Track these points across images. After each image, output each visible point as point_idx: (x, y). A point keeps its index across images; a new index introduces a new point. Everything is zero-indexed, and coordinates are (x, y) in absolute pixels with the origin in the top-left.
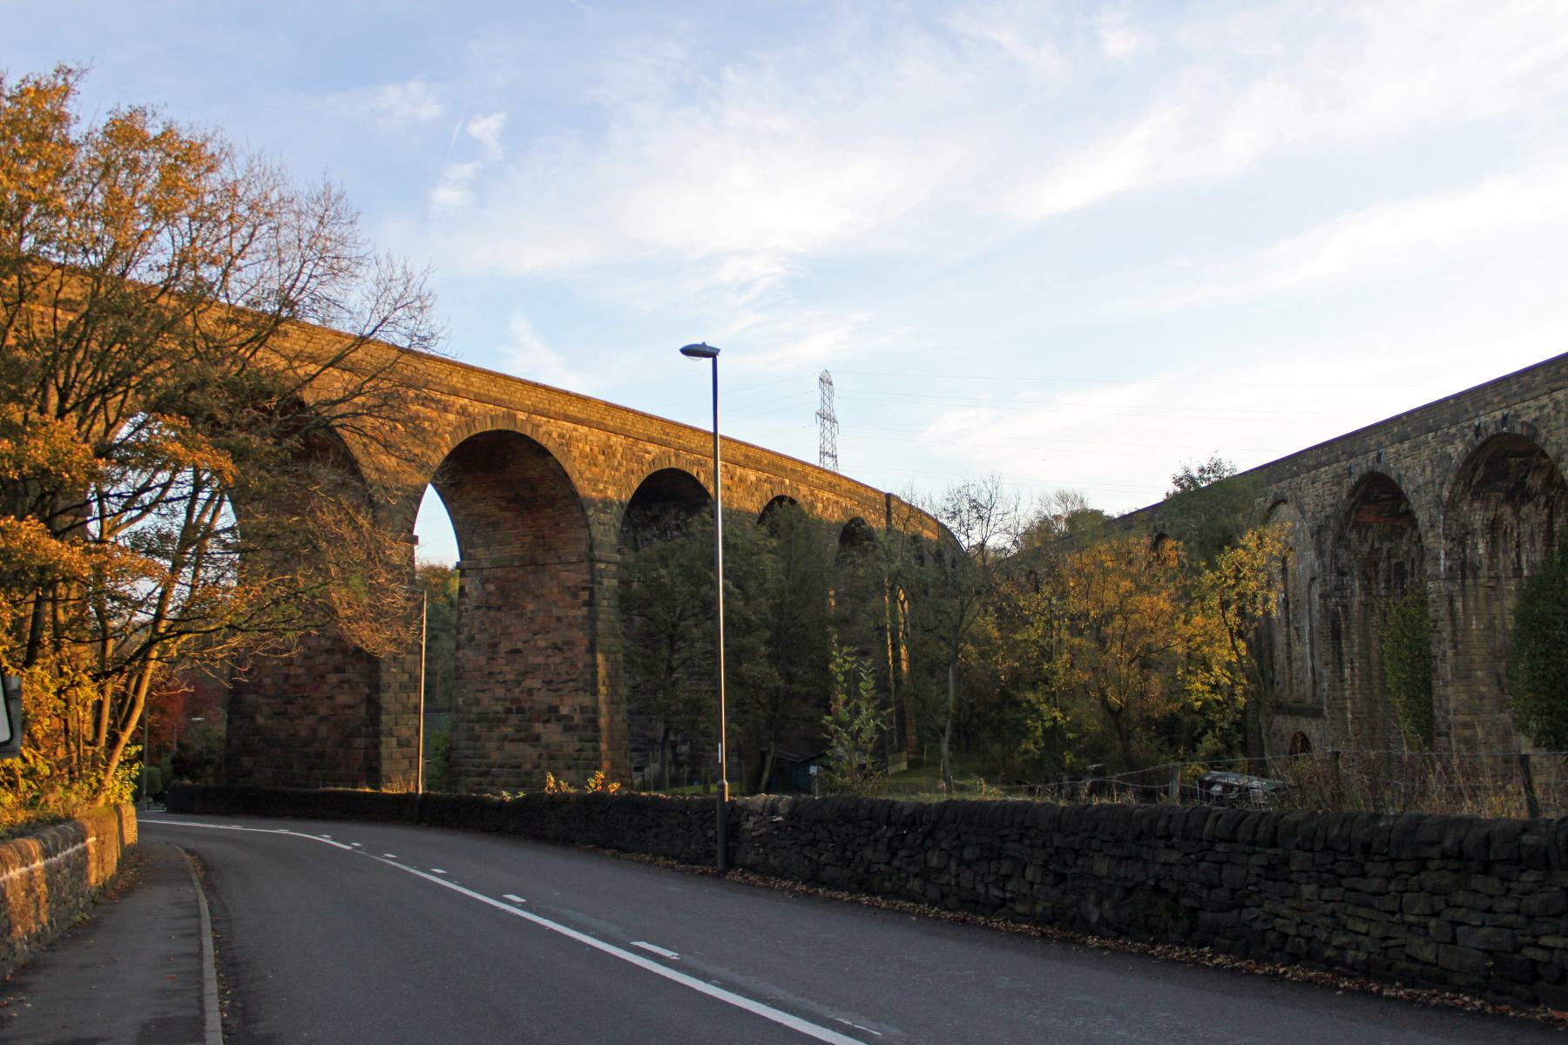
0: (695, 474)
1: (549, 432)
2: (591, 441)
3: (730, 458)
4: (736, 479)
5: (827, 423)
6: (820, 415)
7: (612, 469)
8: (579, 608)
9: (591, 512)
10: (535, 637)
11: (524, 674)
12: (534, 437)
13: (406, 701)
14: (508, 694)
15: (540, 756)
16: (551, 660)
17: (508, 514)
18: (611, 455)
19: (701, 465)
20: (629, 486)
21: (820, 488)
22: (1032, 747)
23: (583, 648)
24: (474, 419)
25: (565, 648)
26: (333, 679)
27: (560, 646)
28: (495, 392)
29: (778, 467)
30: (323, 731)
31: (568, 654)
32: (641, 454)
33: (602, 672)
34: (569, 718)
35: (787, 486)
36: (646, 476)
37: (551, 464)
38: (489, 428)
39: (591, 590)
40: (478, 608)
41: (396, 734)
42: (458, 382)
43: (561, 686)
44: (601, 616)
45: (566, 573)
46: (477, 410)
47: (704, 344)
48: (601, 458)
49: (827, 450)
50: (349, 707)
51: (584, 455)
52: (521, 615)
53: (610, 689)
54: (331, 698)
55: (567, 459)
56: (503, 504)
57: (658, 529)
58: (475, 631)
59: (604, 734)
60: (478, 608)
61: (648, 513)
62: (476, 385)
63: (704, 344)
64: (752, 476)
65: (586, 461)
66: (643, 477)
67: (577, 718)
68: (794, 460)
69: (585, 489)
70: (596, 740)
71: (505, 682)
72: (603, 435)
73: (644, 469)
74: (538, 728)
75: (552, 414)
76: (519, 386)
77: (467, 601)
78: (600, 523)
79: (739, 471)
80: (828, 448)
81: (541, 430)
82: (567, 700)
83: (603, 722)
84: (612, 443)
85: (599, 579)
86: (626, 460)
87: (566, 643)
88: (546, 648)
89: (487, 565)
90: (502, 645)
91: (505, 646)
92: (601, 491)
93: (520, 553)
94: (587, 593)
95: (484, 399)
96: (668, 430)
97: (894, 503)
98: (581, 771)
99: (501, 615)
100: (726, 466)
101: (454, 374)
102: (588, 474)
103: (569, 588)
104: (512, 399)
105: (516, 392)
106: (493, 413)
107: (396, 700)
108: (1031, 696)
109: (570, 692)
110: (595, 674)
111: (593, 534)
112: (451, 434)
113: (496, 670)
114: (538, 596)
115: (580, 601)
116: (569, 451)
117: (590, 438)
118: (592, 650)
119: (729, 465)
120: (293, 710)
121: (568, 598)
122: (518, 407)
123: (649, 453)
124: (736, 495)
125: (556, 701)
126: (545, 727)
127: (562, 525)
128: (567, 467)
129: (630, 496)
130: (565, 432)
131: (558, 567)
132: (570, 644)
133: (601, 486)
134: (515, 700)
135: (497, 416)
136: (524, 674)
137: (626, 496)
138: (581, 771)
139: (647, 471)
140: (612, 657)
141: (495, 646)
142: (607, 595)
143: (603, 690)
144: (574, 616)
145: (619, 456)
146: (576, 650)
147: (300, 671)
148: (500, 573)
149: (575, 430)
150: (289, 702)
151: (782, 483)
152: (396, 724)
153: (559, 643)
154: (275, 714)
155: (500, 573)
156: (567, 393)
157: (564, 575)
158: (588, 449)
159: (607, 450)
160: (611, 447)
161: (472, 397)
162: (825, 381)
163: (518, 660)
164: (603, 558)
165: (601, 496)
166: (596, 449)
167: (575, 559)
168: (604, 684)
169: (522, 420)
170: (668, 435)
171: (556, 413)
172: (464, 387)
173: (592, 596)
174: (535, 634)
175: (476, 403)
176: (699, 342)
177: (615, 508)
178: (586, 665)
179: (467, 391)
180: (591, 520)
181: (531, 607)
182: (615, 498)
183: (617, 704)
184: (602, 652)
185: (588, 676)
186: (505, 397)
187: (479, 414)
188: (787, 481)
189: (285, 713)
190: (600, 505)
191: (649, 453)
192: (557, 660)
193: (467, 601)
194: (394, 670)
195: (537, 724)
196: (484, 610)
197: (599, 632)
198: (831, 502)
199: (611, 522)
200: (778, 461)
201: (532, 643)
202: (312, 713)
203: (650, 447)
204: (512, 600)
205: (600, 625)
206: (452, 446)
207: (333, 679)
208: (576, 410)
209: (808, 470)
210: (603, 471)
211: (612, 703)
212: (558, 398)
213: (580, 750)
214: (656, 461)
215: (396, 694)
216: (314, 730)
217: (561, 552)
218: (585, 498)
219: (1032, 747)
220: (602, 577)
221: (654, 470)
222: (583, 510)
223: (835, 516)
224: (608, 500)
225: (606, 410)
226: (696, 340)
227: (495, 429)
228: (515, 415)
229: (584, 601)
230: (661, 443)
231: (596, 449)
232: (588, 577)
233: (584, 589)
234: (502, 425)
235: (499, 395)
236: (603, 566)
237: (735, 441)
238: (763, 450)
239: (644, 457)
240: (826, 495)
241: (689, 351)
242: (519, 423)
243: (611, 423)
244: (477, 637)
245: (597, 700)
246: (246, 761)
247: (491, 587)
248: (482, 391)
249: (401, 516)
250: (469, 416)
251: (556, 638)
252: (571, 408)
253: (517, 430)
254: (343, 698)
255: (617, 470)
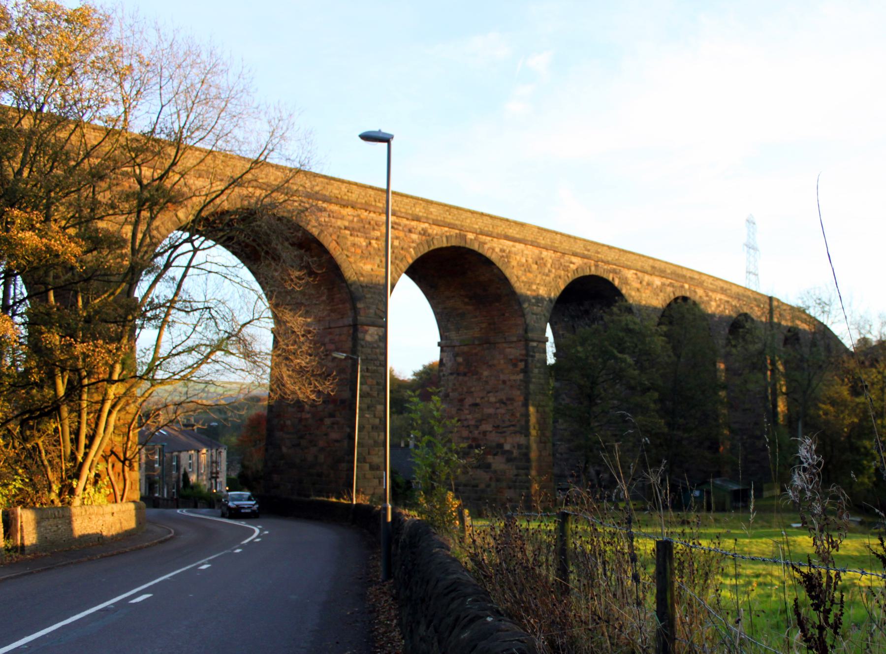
0: (610, 279)
1: (493, 248)
2: (527, 254)
3: (639, 268)
4: (644, 283)
5: (751, 251)
6: (747, 245)
7: (544, 274)
8: (518, 374)
9: (526, 305)
10: (489, 395)
11: (480, 421)
12: (480, 251)
13: (377, 438)
14: (470, 435)
15: (491, 479)
16: (499, 411)
17: (470, 308)
18: (542, 265)
19: (616, 273)
20: (557, 287)
21: (713, 291)
22: (866, 480)
23: (520, 403)
24: (433, 238)
25: (509, 402)
26: (328, 421)
27: (505, 401)
28: (449, 219)
29: (678, 275)
30: (322, 458)
31: (510, 407)
32: (567, 264)
33: (533, 420)
34: (510, 452)
35: (686, 289)
36: (571, 280)
37: (495, 271)
38: (445, 245)
39: (526, 361)
40: (451, 374)
41: (368, 461)
42: (420, 211)
43: (505, 429)
44: (534, 380)
45: (510, 349)
46: (435, 232)
47: (380, 131)
48: (535, 267)
49: (751, 270)
50: (337, 441)
51: (520, 265)
52: (479, 379)
53: (539, 432)
54: (326, 435)
55: (507, 268)
56: (466, 300)
57: (589, 319)
58: (449, 390)
59: (534, 464)
60: (451, 374)
61: (581, 308)
62: (434, 213)
63: (380, 131)
64: (657, 281)
65: (523, 269)
66: (568, 281)
67: (516, 453)
68: (692, 271)
69: (520, 287)
70: (528, 468)
71: (468, 426)
72: (536, 251)
73: (569, 275)
74: (490, 458)
75: (495, 234)
76: (469, 215)
77: (444, 369)
78: (533, 314)
79: (647, 278)
80: (752, 269)
81: (486, 246)
82: (509, 440)
83: (534, 455)
84: (543, 256)
85: (531, 353)
86: (555, 268)
87: (508, 399)
88: (496, 403)
89: (457, 344)
90: (467, 400)
91: (469, 401)
92: (534, 291)
93: (478, 335)
94: (523, 363)
95: (441, 223)
96: (589, 248)
97: (775, 303)
98: (518, 490)
99: (466, 379)
100: (636, 274)
101: (417, 206)
102: (524, 278)
103: (511, 360)
104: (463, 224)
105: (466, 219)
106: (448, 234)
107: (369, 437)
108: (867, 443)
109: (511, 433)
110: (528, 421)
111: (528, 321)
112: (414, 248)
113: (463, 417)
114: (490, 366)
115: (518, 369)
116: (509, 262)
117: (526, 252)
118: (526, 405)
119: (640, 274)
120: (304, 442)
121: (511, 367)
122: (468, 229)
123: (574, 263)
124: (644, 295)
125: (502, 441)
126: (494, 459)
127: (507, 315)
128: (507, 273)
129: (558, 294)
130: (505, 248)
131: (505, 345)
132: (511, 400)
133: (534, 287)
134: (474, 439)
135: (451, 236)
136: (480, 421)
137: (554, 294)
138: (518, 490)
139: (571, 277)
140: (540, 409)
141: (461, 401)
142: (539, 365)
143: (533, 432)
144: (514, 380)
145: (549, 265)
146: (515, 404)
147: (308, 416)
148: (466, 349)
149: (514, 246)
150: (301, 437)
151: (682, 287)
152: (369, 453)
153: (504, 398)
154: (293, 445)
155: (466, 349)
156: (507, 220)
157: (508, 350)
158: (524, 260)
159: (540, 262)
160: (543, 259)
161: (431, 222)
162: (750, 222)
163: (477, 410)
164: (535, 339)
165: (534, 294)
166: (530, 261)
167: (515, 339)
168: (534, 428)
169: (471, 240)
170: (589, 250)
171: (498, 234)
172: (425, 215)
173: (526, 366)
174: (489, 392)
175: (434, 227)
176: (376, 129)
177: (545, 303)
178: (522, 415)
179: (427, 218)
180: (526, 311)
181: (486, 373)
182: (546, 296)
183: (545, 443)
184: (533, 405)
185: (523, 423)
186: (457, 222)
187: (437, 234)
188: (686, 286)
189: (299, 445)
190: (533, 301)
191: (574, 263)
192: (502, 411)
193: (444, 369)
194: (367, 416)
195: (489, 457)
196: (455, 376)
197: (531, 392)
198: (723, 301)
199: (542, 313)
200: (679, 271)
201: (486, 399)
202: (315, 445)
203: (574, 259)
204: (473, 368)
205: (532, 387)
206: (415, 258)
207: (328, 421)
208: (515, 232)
209: (704, 278)
210: (536, 276)
211: (541, 442)
212: (499, 223)
213: (516, 475)
214: (579, 270)
215: (369, 433)
216: (316, 457)
217: (507, 334)
218: (522, 295)
219: (866, 480)
220: (534, 352)
221: (577, 276)
222: (520, 304)
223: (658, 302)
224: (540, 297)
225: (539, 232)
226: (372, 127)
227: (449, 245)
228: (465, 236)
229: (522, 369)
230: (584, 257)
231: (530, 261)
232: (524, 352)
233: (521, 361)
234: (454, 243)
235: (452, 221)
236: (535, 344)
237: (644, 256)
238: (666, 263)
239: (569, 266)
240: (719, 296)
241: (367, 137)
242: (468, 241)
243: (543, 242)
244: (451, 394)
245: (529, 439)
246: (276, 478)
247: (460, 360)
248: (439, 218)
249: (374, 307)
250: (429, 235)
251: (502, 396)
252: (511, 231)
253: (467, 246)
254: (334, 435)
255: (547, 275)
